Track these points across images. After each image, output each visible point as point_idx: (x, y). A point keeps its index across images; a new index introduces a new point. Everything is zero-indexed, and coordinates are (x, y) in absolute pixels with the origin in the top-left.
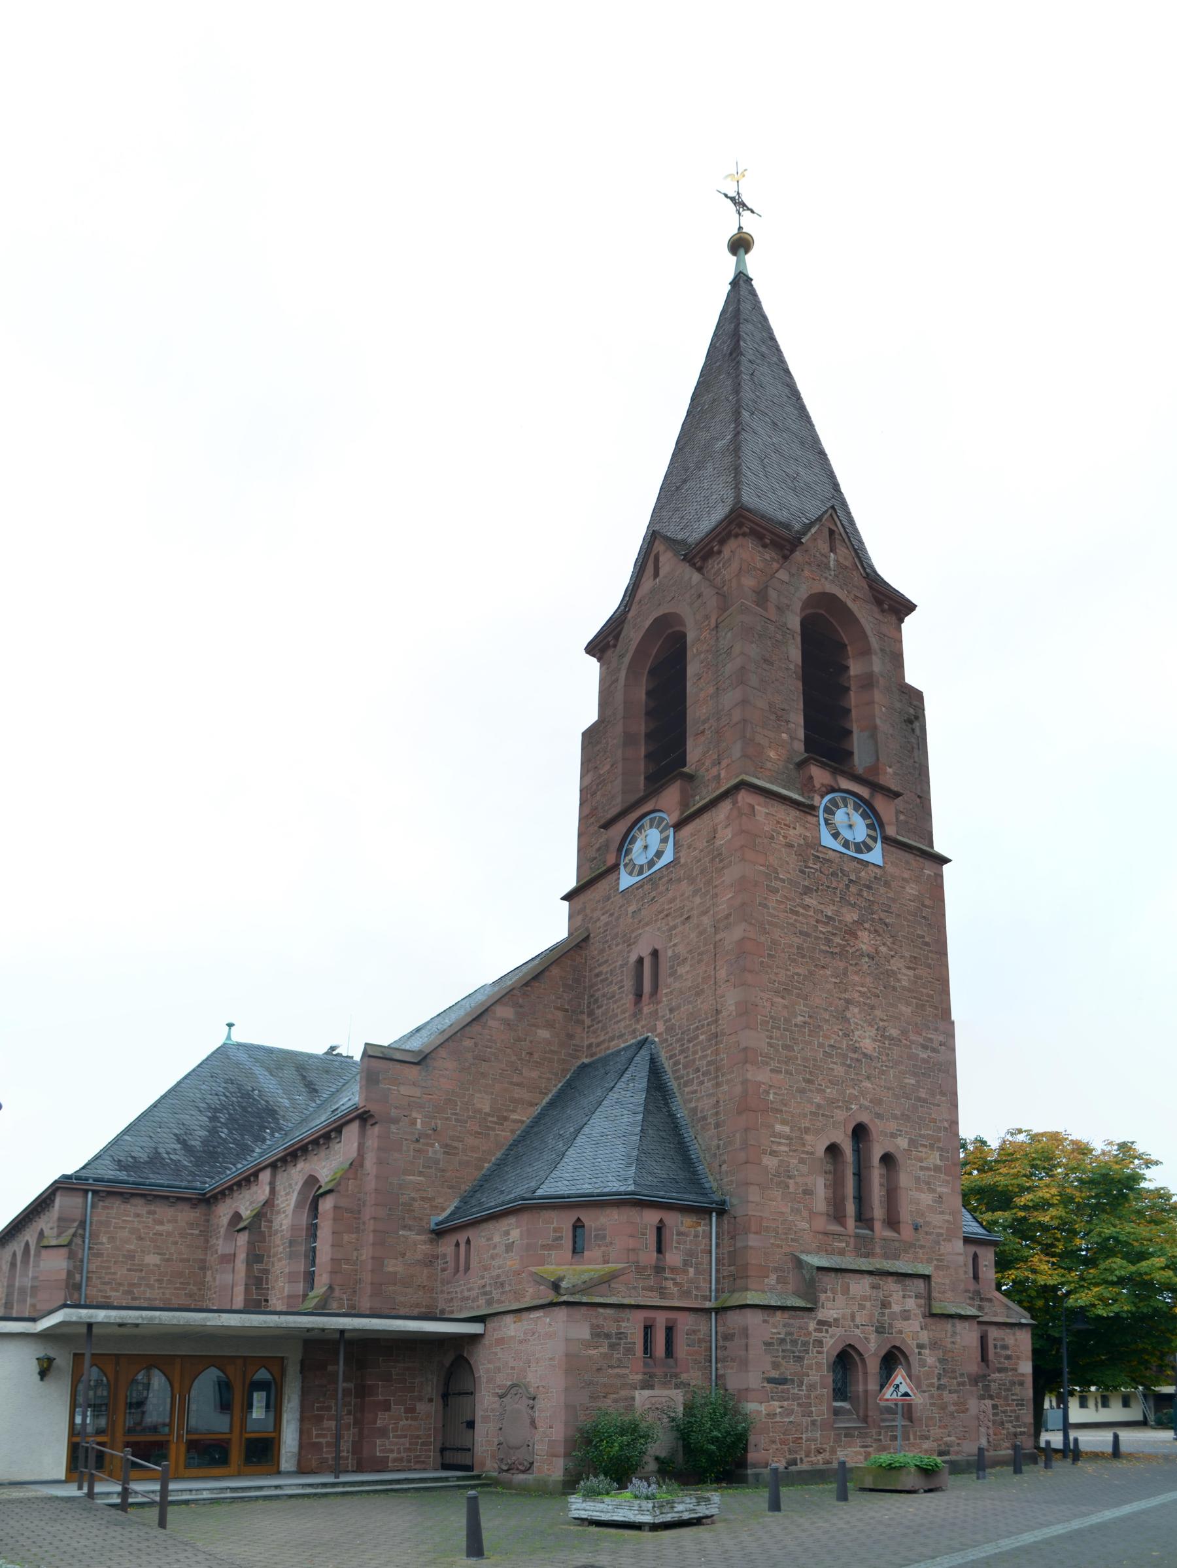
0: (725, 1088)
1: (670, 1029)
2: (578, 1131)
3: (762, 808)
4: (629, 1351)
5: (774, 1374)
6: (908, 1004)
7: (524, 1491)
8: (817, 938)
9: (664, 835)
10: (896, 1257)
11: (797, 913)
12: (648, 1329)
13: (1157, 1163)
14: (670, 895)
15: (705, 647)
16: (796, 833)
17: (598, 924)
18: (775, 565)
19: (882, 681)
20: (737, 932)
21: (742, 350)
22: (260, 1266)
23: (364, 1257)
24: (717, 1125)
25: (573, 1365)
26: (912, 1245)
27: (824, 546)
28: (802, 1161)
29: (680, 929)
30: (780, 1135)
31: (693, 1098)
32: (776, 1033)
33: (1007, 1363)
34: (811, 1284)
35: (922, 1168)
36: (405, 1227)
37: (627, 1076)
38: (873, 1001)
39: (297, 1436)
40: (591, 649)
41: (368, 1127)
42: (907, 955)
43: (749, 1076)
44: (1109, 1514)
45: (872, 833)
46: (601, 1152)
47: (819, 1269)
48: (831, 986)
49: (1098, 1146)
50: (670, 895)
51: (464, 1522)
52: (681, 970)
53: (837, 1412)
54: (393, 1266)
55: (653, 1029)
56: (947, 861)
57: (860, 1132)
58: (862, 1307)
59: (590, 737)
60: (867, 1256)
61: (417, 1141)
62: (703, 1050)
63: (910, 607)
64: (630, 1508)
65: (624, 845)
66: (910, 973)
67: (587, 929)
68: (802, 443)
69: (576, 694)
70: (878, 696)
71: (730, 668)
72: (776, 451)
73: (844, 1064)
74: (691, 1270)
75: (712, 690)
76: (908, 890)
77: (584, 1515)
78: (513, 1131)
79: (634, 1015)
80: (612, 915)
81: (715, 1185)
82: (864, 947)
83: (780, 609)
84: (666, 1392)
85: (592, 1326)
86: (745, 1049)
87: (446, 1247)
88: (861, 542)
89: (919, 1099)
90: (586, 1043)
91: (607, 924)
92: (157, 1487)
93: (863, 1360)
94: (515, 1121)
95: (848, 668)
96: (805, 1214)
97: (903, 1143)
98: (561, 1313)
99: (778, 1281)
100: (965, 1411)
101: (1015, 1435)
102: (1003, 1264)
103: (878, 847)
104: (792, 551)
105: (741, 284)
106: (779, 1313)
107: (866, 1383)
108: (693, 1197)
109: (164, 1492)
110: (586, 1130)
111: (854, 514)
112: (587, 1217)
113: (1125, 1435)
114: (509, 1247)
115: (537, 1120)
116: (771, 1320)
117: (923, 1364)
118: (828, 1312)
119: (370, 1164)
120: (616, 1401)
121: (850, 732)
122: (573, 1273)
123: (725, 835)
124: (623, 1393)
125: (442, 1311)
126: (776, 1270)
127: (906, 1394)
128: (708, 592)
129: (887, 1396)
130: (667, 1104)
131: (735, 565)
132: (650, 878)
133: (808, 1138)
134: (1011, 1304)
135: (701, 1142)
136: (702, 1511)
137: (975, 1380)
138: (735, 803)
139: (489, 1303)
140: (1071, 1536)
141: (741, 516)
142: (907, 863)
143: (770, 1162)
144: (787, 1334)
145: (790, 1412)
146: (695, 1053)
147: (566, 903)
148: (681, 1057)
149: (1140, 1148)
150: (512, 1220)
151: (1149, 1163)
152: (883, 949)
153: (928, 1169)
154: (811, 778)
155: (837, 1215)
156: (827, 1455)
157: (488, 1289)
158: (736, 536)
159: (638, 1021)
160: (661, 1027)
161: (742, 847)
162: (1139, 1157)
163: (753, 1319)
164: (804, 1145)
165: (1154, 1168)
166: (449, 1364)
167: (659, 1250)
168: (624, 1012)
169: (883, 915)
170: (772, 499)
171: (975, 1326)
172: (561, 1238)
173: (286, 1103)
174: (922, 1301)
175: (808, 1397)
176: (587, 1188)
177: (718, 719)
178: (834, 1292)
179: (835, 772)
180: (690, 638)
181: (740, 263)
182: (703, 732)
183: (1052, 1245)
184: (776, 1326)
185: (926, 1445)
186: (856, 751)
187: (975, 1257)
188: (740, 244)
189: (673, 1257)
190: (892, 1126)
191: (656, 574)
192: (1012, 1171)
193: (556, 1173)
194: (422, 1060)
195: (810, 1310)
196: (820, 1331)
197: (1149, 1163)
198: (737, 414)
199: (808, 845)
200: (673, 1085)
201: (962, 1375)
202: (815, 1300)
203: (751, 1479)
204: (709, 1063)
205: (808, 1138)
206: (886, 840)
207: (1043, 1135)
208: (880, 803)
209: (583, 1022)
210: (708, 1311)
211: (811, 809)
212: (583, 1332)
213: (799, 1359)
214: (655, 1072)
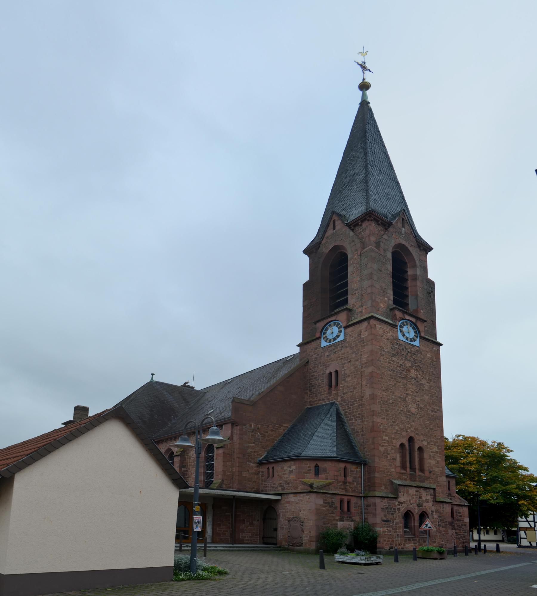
0: (365, 423)
1: (343, 400)
2: (313, 434)
3: (379, 326)
4: (336, 509)
5: (385, 519)
6: (427, 395)
7: (300, 552)
8: (397, 372)
9: (340, 329)
10: (423, 482)
11: (390, 363)
12: (342, 501)
13: (512, 451)
14: (342, 352)
15: (355, 262)
16: (390, 335)
17: (312, 357)
18: (382, 232)
19: (420, 278)
20: (370, 369)
21: (364, 134)
22: (184, 469)
23: (234, 471)
24: (363, 435)
25: (318, 512)
26: (429, 478)
27: (400, 225)
28: (392, 449)
29: (347, 364)
30: (385, 440)
31: (354, 425)
32: (383, 406)
33: (460, 518)
34: (395, 491)
35: (431, 452)
36: (249, 461)
37: (328, 416)
38: (415, 394)
39: (211, 530)
40: (306, 252)
41: (234, 426)
42: (427, 378)
43: (375, 420)
44: (505, 568)
45: (416, 335)
46: (321, 441)
47: (399, 485)
48: (401, 389)
49: (490, 443)
50: (342, 352)
52: (347, 379)
53: (405, 532)
54: (245, 474)
55: (337, 399)
56: (441, 345)
57: (411, 440)
58: (413, 498)
60: (414, 481)
61: (252, 432)
62: (357, 409)
64: (357, 558)
65: (323, 330)
66: (428, 385)
67: (308, 358)
68: (390, 179)
69: (301, 270)
70: (419, 284)
71: (366, 272)
72: (381, 183)
73: (405, 417)
74: (355, 483)
75: (359, 279)
76: (428, 355)
77: (340, 560)
78: (284, 430)
79: (329, 393)
80: (318, 355)
81: (362, 455)
82: (413, 375)
83: (385, 250)
84: (348, 523)
85: (324, 500)
86: (373, 411)
87: (264, 469)
88: (412, 221)
89: (430, 429)
90: (308, 400)
91: (316, 358)
92: (203, 545)
93: (413, 515)
94: (285, 427)
95: (407, 272)
96: (393, 466)
97: (425, 443)
98: (313, 496)
99: (385, 488)
100: (448, 534)
101: (464, 542)
102: (457, 484)
103: (418, 340)
104: (389, 227)
105: (365, 109)
106: (386, 499)
107: (414, 523)
108: (355, 459)
109: (205, 547)
110: (316, 434)
111: (410, 209)
112: (320, 464)
113: (502, 545)
114: (291, 472)
115: (293, 427)
116: (383, 501)
117: (433, 517)
118: (402, 499)
119: (235, 438)
120: (331, 525)
121: (407, 296)
122: (317, 482)
123: (365, 334)
124: (334, 522)
125: (262, 491)
126: (384, 485)
127: (430, 527)
128: (357, 240)
129: (423, 527)
130: (343, 426)
131: (368, 232)
132: (334, 344)
133: (394, 441)
134: (461, 498)
135: (357, 440)
136: (378, 560)
137: (451, 524)
138: (369, 323)
139: (283, 489)
140: (496, 572)
141: (371, 213)
142: (428, 345)
143: (382, 449)
144: (389, 506)
145: (390, 531)
146: (353, 410)
147: (299, 348)
148: (348, 410)
149: (506, 445)
150: (292, 463)
151: (509, 451)
152: (419, 376)
153: (434, 452)
154: (395, 315)
155: (403, 467)
156: (402, 546)
157: (282, 484)
158: (368, 220)
159: (330, 396)
160: (339, 399)
161: (372, 339)
162: (505, 448)
163: (378, 501)
164: (393, 443)
165: (511, 453)
166: (268, 510)
167: (345, 476)
168: (324, 391)
169: (419, 364)
170: (381, 205)
171: (450, 506)
172: (310, 470)
173: (178, 406)
174: (432, 497)
175: (396, 527)
176: (319, 454)
177: (362, 290)
178: (403, 492)
179: (404, 313)
180: (349, 256)
181: (364, 96)
182: (355, 294)
183: (474, 478)
184: (384, 503)
185: (435, 544)
186: (410, 303)
187: (449, 482)
188: (364, 87)
189: (350, 479)
190: (421, 438)
191: (334, 228)
192: (459, 451)
193: (308, 448)
194: (253, 404)
195: (396, 498)
196: (399, 505)
197: (509, 451)
198: (366, 166)
199: (394, 339)
200: (345, 419)
201: (446, 522)
202: (398, 495)
203: (378, 552)
204: (359, 414)
205: (394, 441)
206: (421, 337)
207: (469, 437)
208: (419, 324)
209: (307, 393)
210: (361, 497)
211: (395, 326)
212: (321, 502)
213: (393, 514)
214: (338, 415)
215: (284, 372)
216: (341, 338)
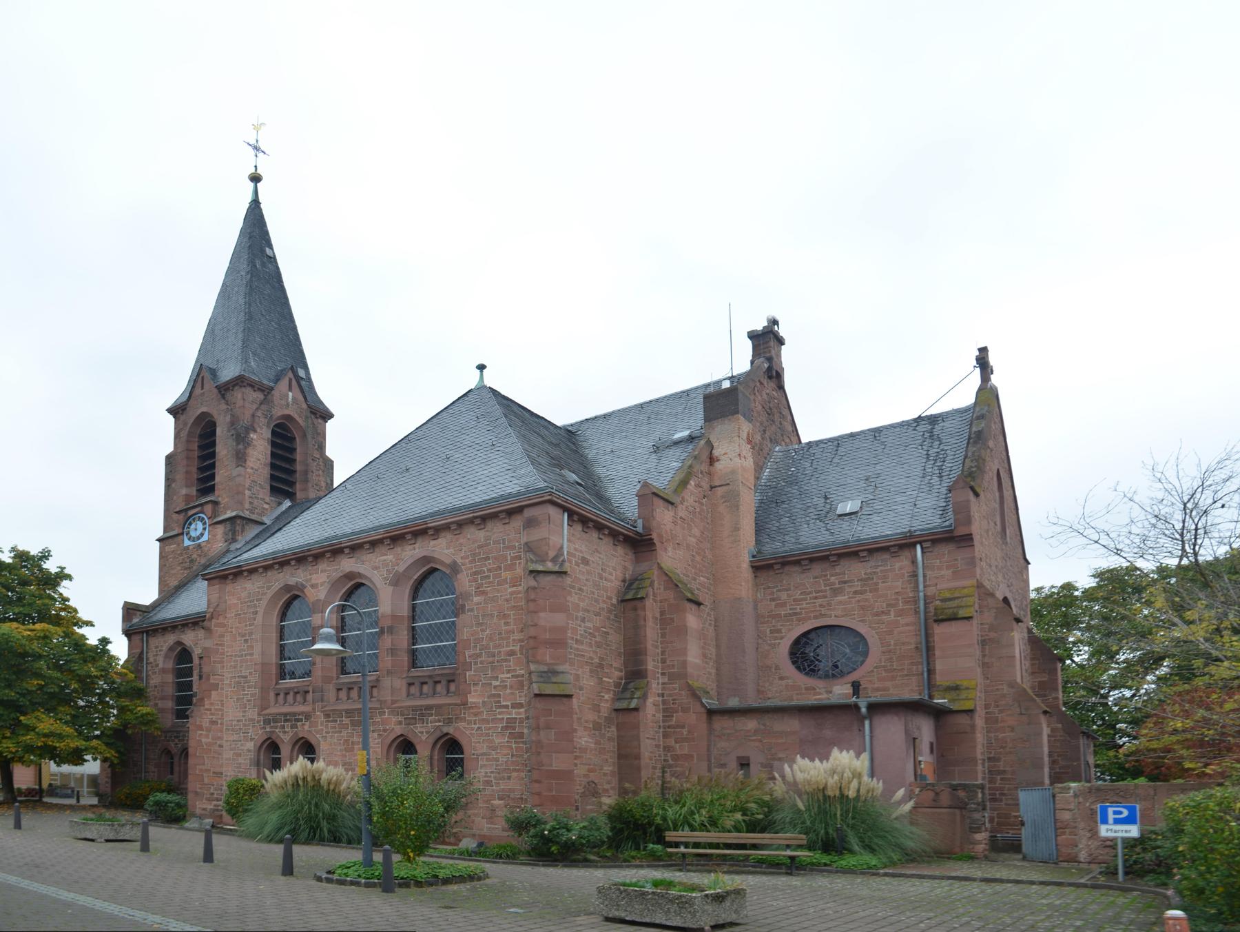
40: (170, 411)
51: (202, 842)
59: (169, 458)
63: (331, 416)
69: (162, 437)
105: (255, 205)
188: (256, 179)
215: (244, 266)
216: (205, 538)
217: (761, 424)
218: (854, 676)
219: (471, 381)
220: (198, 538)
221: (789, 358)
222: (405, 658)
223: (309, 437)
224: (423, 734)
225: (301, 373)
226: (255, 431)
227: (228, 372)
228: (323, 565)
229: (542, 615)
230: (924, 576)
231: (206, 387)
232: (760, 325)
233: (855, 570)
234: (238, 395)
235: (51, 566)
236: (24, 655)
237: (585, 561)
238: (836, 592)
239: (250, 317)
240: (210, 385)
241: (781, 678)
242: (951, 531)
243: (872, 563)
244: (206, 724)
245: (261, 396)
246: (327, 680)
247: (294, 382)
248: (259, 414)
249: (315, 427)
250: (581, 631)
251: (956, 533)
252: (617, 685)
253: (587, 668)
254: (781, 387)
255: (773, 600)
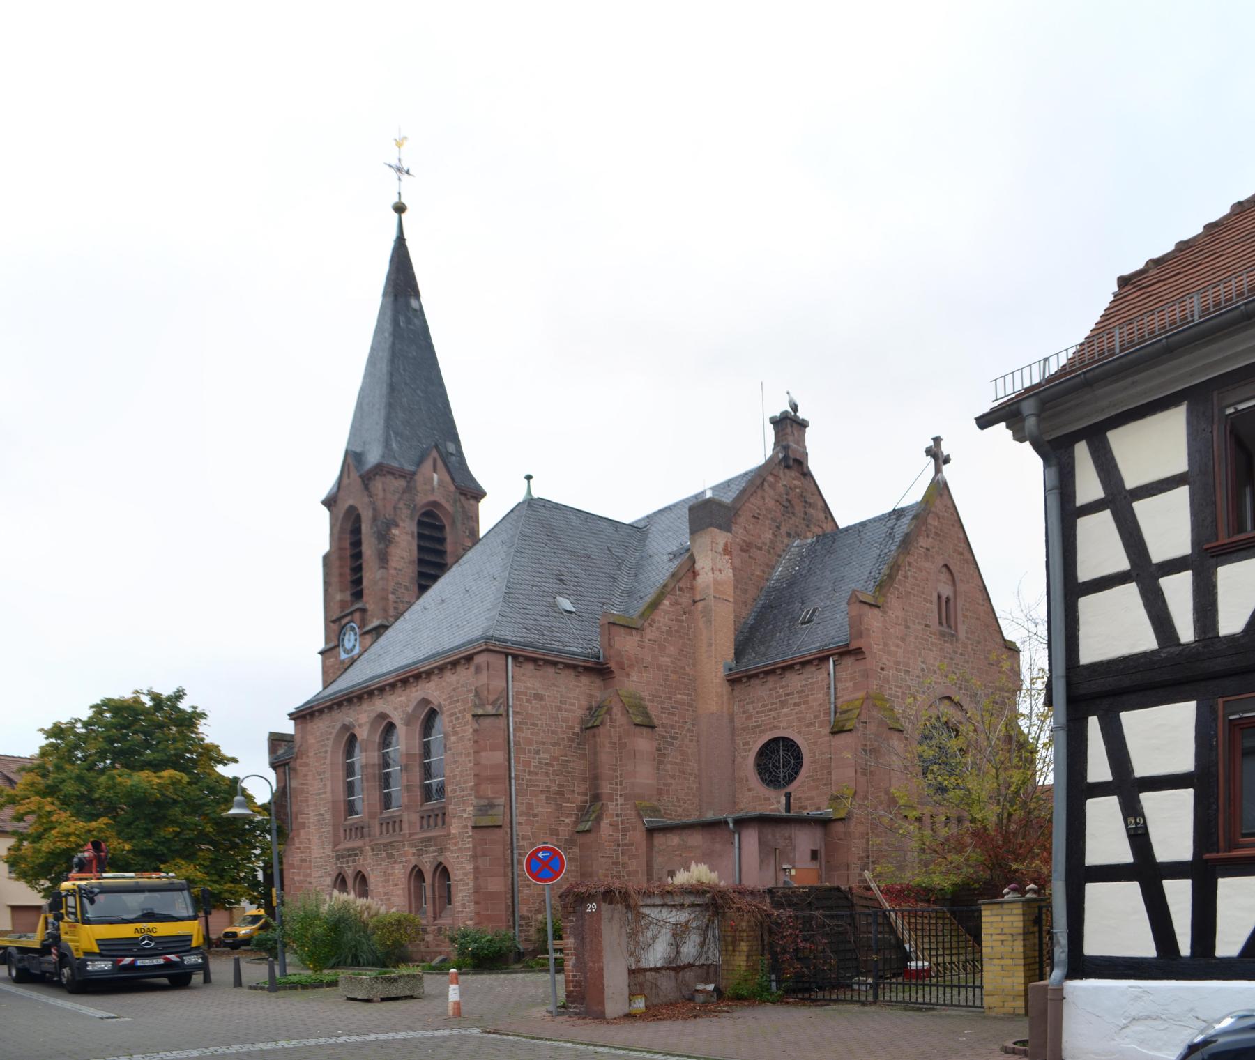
59: (326, 559)
63: (483, 494)
69: (317, 533)
188: (400, 209)
217: (774, 520)
218: (788, 789)
219: (520, 497)
220: (352, 650)
221: (812, 440)
222: (418, 793)
223: (459, 525)
224: (349, 873)
225: (451, 448)
226: (397, 526)
227: (373, 457)
228: (365, 706)
229: (483, 754)
230: (835, 688)
231: (352, 475)
232: (779, 407)
233: (794, 681)
234: (378, 485)
235: (184, 705)
236: (158, 804)
237: (538, 697)
238: (783, 704)
239: (392, 388)
240: (355, 475)
241: (749, 790)
242: (847, 645)
243: (804, 676)
244: (297, 863)
245: (402, 483)
246: (372, 816)
247: (440, 463)
248: (401, 505)
249: (465, 512)
250: (535, 762)
251: (851, 648)
252: (580, 808)
253: (543, 797)
254: (807, 475)
255: (744, 712)
